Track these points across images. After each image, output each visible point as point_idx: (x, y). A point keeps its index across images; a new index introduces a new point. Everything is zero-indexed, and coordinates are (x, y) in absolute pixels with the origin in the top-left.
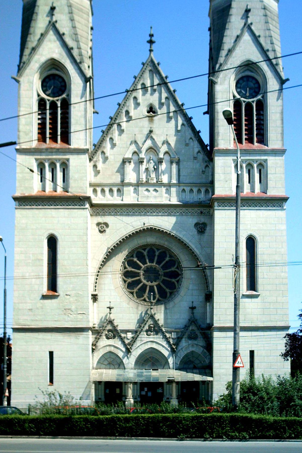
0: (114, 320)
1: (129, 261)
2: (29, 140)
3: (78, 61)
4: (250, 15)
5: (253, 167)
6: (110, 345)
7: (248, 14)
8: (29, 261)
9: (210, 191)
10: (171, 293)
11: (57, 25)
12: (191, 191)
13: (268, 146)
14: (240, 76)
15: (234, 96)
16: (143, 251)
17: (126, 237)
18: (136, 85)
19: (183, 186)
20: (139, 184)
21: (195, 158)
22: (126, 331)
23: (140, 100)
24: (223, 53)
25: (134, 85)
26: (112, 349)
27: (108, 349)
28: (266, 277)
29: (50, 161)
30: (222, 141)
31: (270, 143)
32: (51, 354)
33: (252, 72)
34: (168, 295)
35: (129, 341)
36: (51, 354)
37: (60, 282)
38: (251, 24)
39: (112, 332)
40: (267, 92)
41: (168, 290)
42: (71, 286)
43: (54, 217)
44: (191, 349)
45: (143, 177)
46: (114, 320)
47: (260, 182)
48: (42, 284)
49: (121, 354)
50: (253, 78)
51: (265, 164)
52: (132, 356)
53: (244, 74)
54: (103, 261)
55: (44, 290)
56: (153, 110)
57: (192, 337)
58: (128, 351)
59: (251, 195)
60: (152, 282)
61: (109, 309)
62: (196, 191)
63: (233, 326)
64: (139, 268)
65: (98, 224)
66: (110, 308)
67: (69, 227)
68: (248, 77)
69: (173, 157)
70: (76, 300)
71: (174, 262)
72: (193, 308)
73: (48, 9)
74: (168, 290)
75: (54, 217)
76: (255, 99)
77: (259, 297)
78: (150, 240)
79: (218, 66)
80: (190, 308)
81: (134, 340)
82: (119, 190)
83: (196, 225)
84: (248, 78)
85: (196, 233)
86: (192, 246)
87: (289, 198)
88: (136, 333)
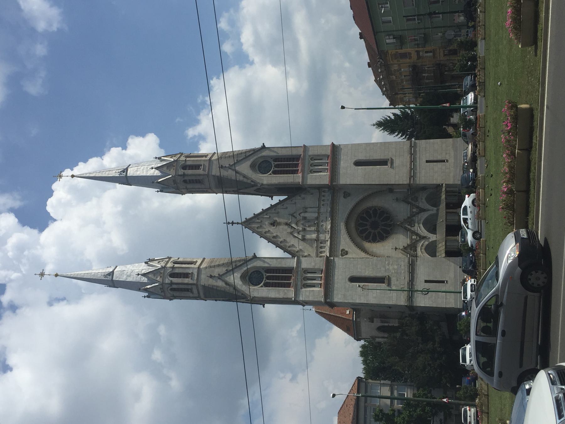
0: (404, 246)
1: (367, 239)
2: (366, 108)
3: (253, 152)
4: (224, 166)
5: (313, 163)
6: (421, 249)
7: (224, 167)
8: (365, 294)
9: (324, 190)
10: (387, 214)
11: (221, 274)
12: (323, 200)
13: (301, 155)
14: (258, 171)
15: (270, 174)
16: (363, 215)
17: (351, 238)
18: (258, 232)
19: (320, 205)
20: (318, 231)
21: (304, 199)
22: (411, 239)
23: (267, 230)
24: (245, 180)
25: (258, 233)
26: (423, 247)
27: (423, 250)
28: (380, 155)
29: (310, 160)
30: (296, 180)
31: (299, 153)
32: (427, 162)
33: (256, 165)
34: (388, 215)
35: (418, 237)
36: (427, 162)
37: (379, 275)
38: (229, 165)
39: (412, 248)
40: (238, 194)
41: (385, 215)
42: (382, 268)
43: (338, 278)
44: (424, 200)
45: (313, 228)
46: (404, 246)
47: (321, 159)
48: (380, 286)
49: (427, 243)
50: (260, 164)
51: (311, 156)
52: (428, 236)
53: (257, 169)
54: (366, 253)
55: (383, 286)
56: (273, 223)
57: (416, 199)
58: (424, 238)
59: (329, 164)
60: (379, 228)
61: (397, 250)
62: (324, 198)
63: (390, 400)
64: (370, 233)
65: (342, 255)
66: (396, 249)
67: (345, 268)
68: (259, 167)
69: (302, 211)
70: (391, 265)
71: (367, 211)
72: (397, 199)
73: (211, 280)
74: (385, 215)
75: (338, 278)
76: (273, 163)
77: (393, 158)
78: (353, 225)
79: (252, 183)
80: (397, 201)
81: (417, 234)
82: (321, 243)
83: (344, 197)
84: (260, 167)
85: (349, 197)
86: (357, 199)
87: (333, 143)
88: (414, 233)
